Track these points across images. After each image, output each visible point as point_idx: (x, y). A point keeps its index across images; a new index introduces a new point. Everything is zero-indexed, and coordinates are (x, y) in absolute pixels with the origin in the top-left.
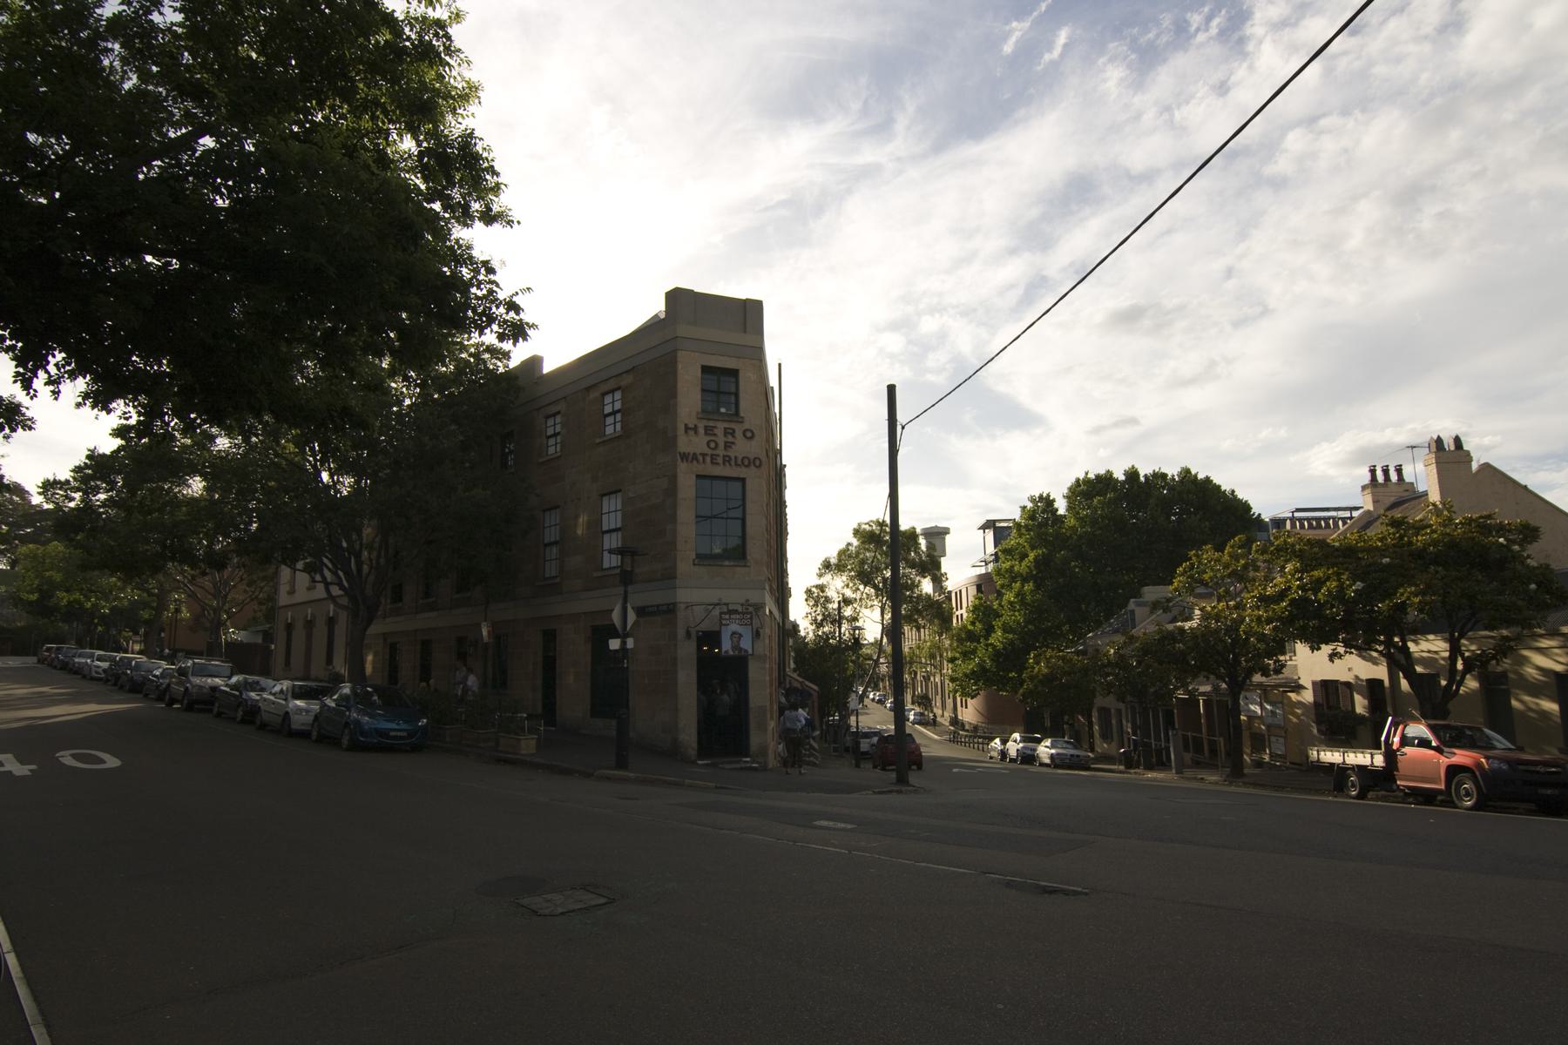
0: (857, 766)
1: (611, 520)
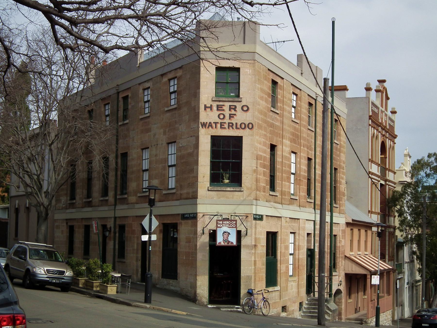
0: (147, 300)
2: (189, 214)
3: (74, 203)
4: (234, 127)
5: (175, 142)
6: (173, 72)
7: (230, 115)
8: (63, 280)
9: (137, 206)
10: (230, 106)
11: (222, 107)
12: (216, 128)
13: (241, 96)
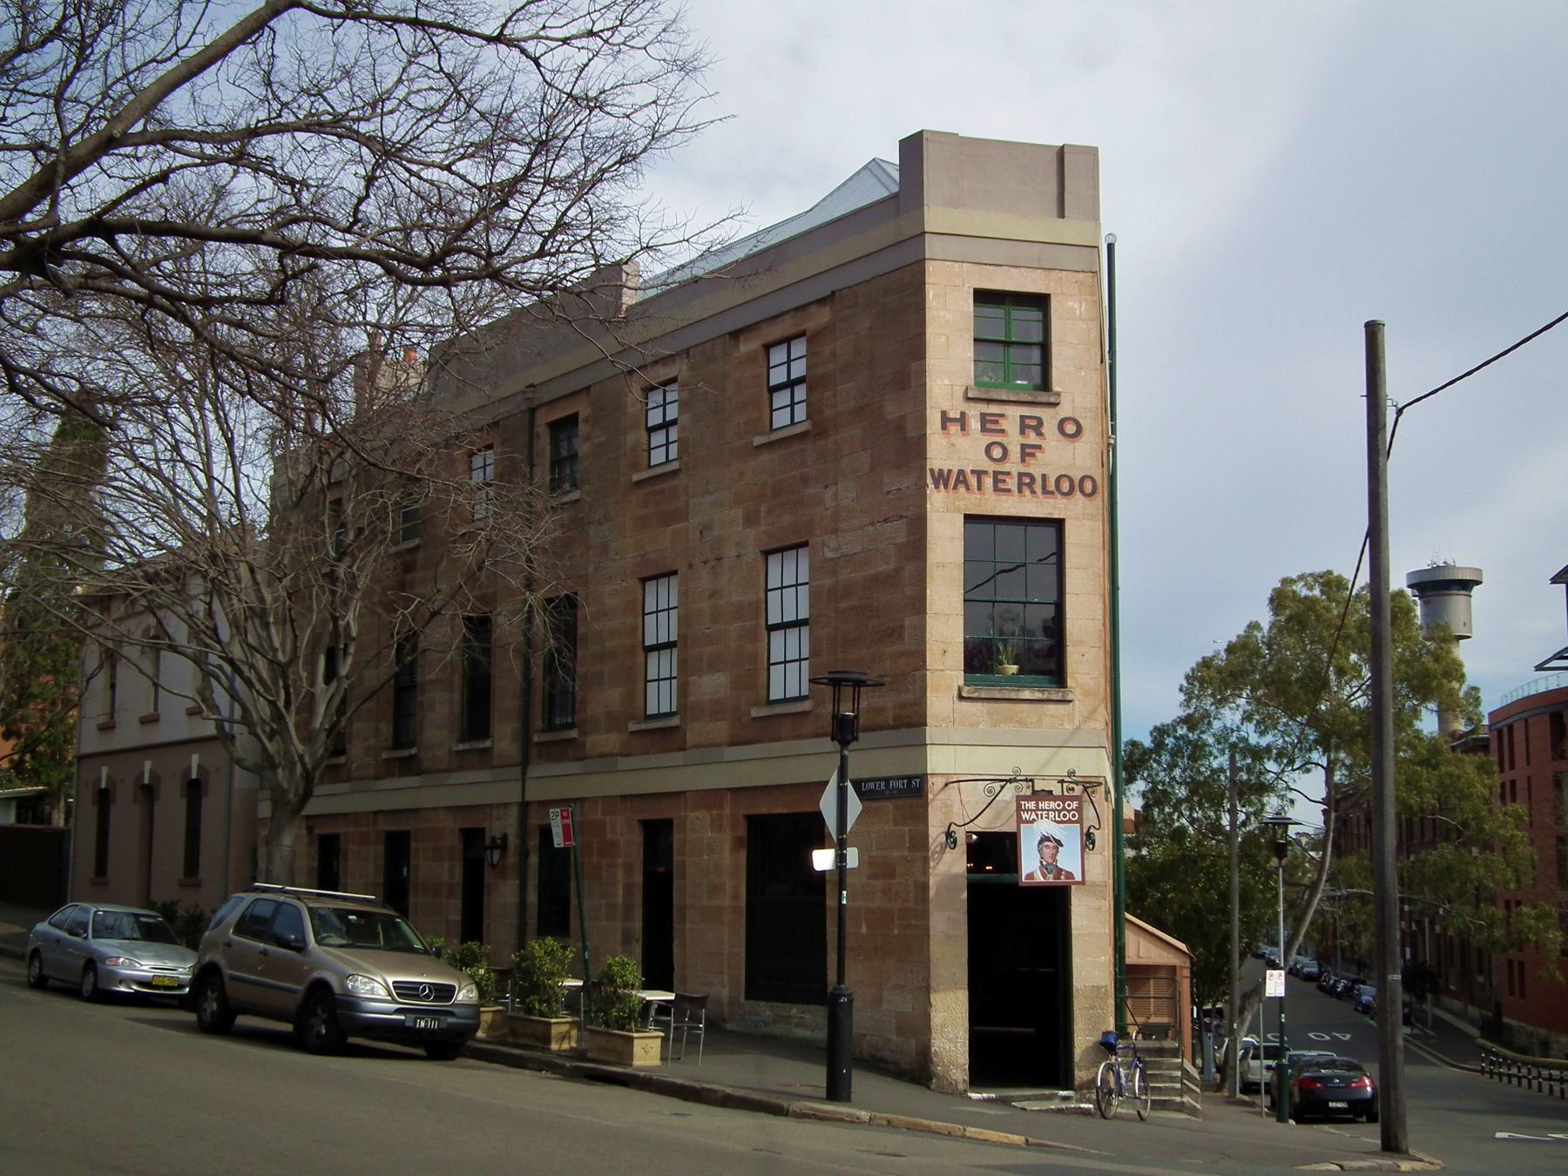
1: (789, 603)
2: (887, 780)
3: (341, 765)
4: (1038, 487)
5: (805, 544)
6: (787, 318)
7: (1023, 447)
8: (450, 1020)
9: (623, 763)
10: (1022, 418)
11: (997, 422)
12: (979, 488)
13: (1056, 388)
